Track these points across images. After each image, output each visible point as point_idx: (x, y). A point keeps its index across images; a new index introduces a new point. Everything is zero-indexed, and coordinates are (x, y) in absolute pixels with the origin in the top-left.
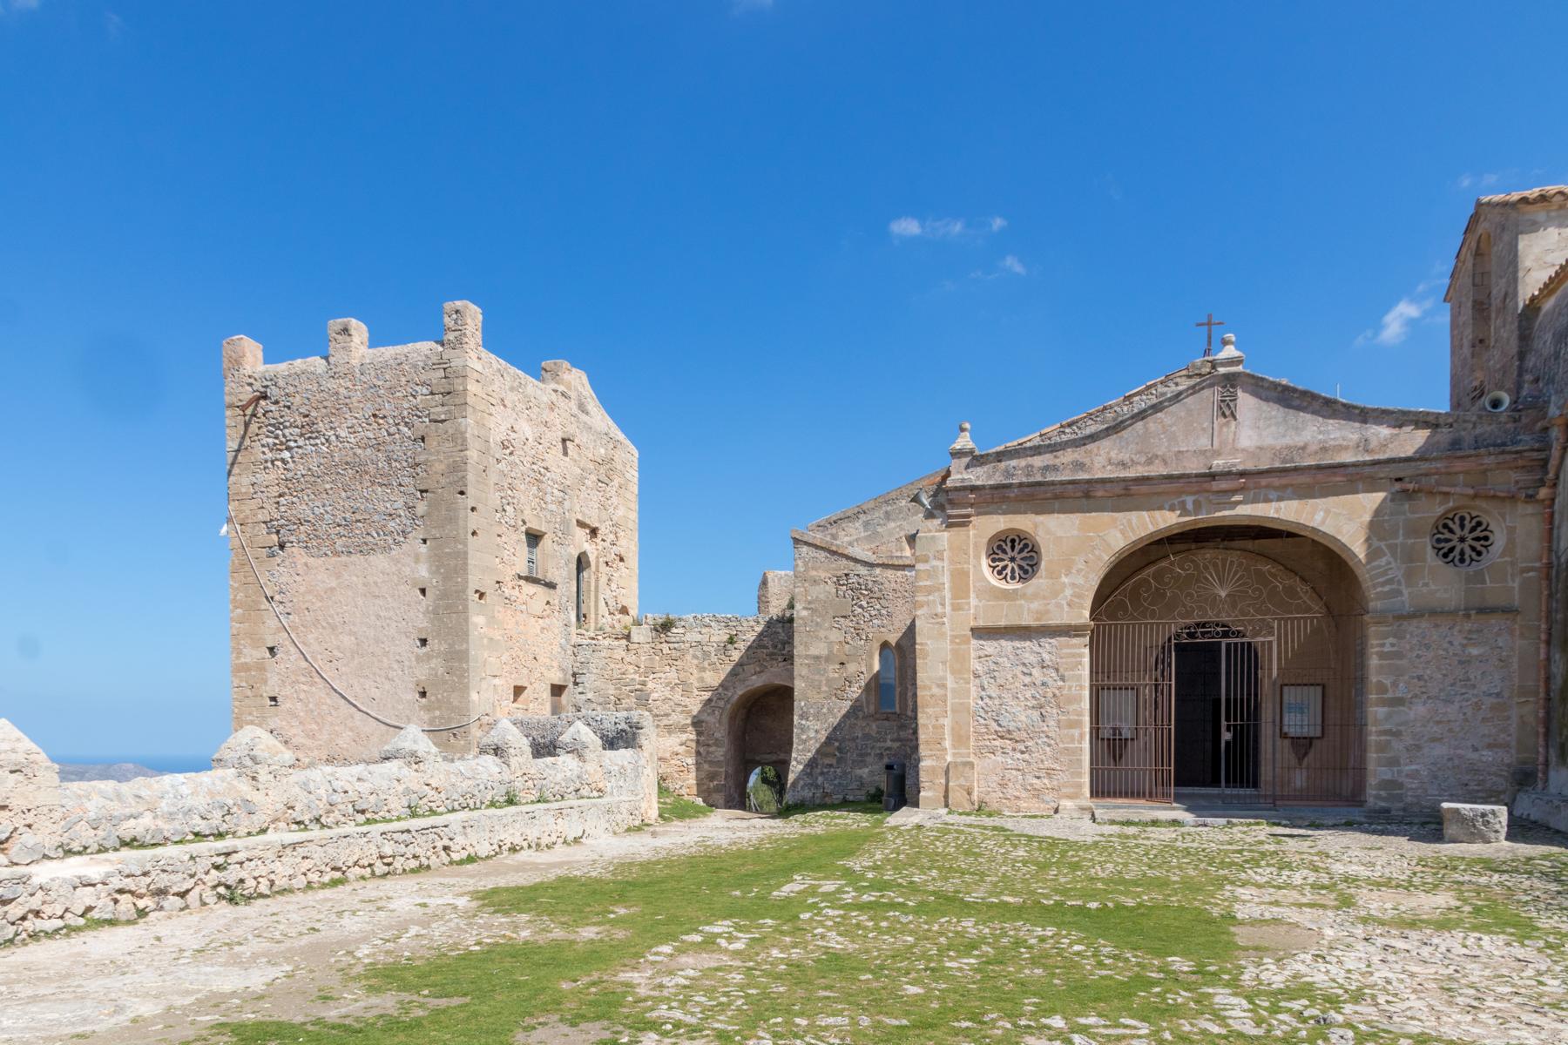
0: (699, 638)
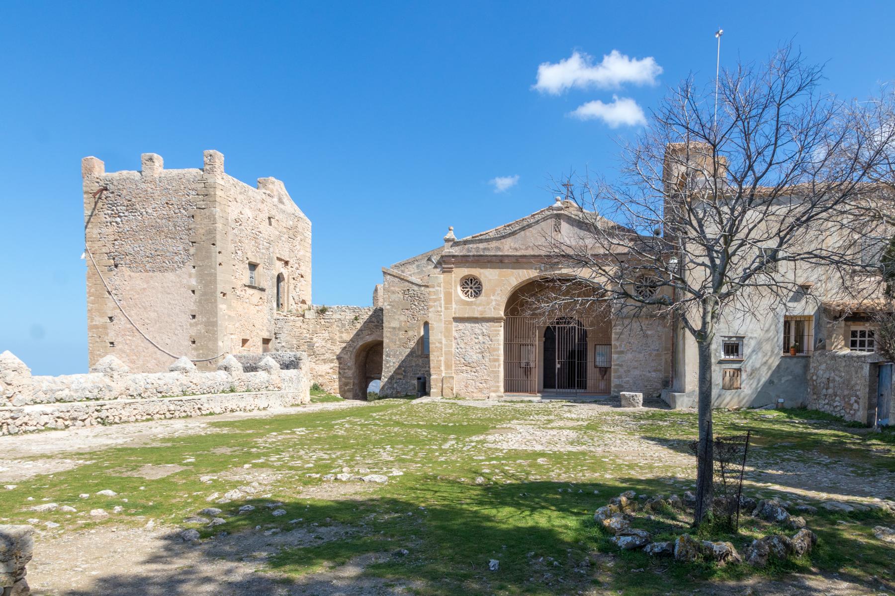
0: (340, 317)
